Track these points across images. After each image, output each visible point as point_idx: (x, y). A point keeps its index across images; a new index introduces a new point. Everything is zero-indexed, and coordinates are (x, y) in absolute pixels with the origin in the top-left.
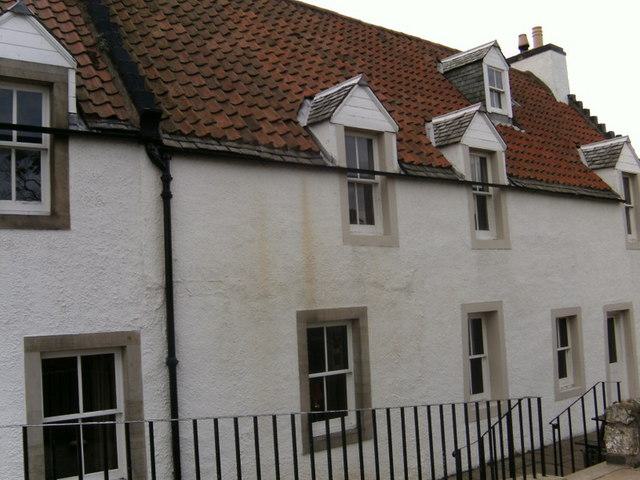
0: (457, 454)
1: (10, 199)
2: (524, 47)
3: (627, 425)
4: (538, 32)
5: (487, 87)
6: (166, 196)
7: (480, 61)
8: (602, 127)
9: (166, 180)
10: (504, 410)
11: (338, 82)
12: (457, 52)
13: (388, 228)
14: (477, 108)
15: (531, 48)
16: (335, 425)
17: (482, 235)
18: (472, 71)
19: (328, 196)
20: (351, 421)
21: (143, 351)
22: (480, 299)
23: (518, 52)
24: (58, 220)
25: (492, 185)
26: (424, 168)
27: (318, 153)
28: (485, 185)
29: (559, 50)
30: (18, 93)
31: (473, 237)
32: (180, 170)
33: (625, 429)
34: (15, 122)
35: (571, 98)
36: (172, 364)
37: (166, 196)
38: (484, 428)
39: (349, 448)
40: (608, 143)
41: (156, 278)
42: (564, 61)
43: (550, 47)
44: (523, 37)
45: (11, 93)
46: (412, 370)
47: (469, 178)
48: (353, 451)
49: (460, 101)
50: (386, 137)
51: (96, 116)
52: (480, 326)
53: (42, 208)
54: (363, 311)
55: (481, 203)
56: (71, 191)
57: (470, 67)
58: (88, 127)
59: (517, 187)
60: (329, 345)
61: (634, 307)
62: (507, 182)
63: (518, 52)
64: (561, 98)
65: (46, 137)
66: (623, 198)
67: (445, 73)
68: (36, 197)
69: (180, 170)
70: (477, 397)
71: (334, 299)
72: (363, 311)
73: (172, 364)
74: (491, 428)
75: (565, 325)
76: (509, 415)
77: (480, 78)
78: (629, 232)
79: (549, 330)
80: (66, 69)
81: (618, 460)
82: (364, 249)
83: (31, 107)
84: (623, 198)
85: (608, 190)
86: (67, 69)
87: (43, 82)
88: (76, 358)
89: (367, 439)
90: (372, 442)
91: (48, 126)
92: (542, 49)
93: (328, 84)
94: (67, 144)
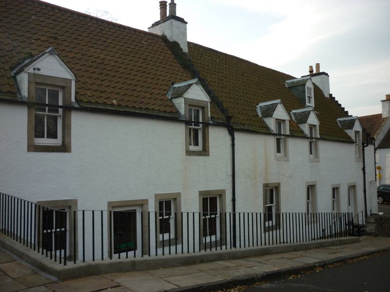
0: (323, 231)
1: (44, 137)
2: (311, 71)
3: (374, 223)
4: (318, 66)
5: (307, 95)
6: (233, 145)
7: (305, 85)
8: (347, 112)
9: (233, 140)
10: (340, 217)
11: (186, 80)
12: (295, 78)
13: (286, 155)
14: (195, 82)
15: (315, 72)
16: (166, 236)
17: (278, 154)
18: (301, 88)
19: (271, 141)
20: (173, 236)
21: (227, 196)
22: (310, 180)
23: (309, 74)
24: (65, 148)
25: (314, 138)
26: (296, 133)
27: (16, 93)
28: (280, 135)
29: (326, 74)
30: (49, 90)
31: (309, 156)
32: (237, 136)
33: (373, 224)
34: (47, 103)
35: (331, 95)
36: (234, 200)
37: (233, 145)
38: (336, 220)
39: (209, 241)
40: (349, 118)
41: (230, 172)
42: (328, 79)
43: (323, 73)
44: (311, 67)
45: (45, 90)
46: (292, 203)
47: (275, 132)
48: (173, 248)
49: (186, 78)
50: (286, 121)
51: (82, 101)
52: (311, 189)
53: (57, 142)
54: (279, 184)
55: (278, 141)
56: (26, 131)
57: (300, 87)
58: (80, 106)
59: (322, 139)
60: (272, 192)
61: (182, 198)
62: (319, 136)
63: (309, 74)
64: (327, 95)
65: (60, 110)
66: (309, 136)
67: (288, 88)
68: (55, 137)
69: (237, 136)
70: (334, 212)
71: (273, 180)
72: (279, 184)
73: (234, 200)
74: (335, 222)
75: (335, 190)
76: (341, 218)
77: (304, 92)
78: (311, 153)
79: (330, 192)
80: (208, 102)
81: (370, 234)
82: (280, 162)
83: (54, 96)
84: (355, 141)
85: (350, 138)
86: (71, 80)
87: (64, 86)
88: (207, 198)
89: (166, 246)
90: (181, 245)
91: (61, 105)
92: (319, 74)
93: (181, 81)
94: (208, 127)
